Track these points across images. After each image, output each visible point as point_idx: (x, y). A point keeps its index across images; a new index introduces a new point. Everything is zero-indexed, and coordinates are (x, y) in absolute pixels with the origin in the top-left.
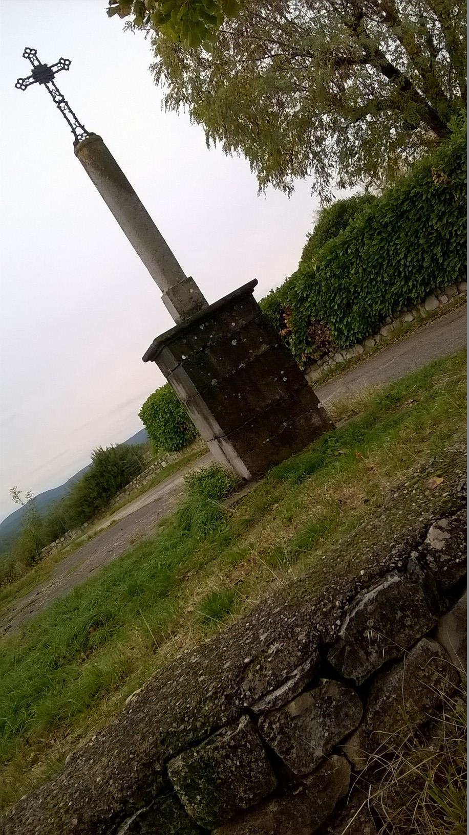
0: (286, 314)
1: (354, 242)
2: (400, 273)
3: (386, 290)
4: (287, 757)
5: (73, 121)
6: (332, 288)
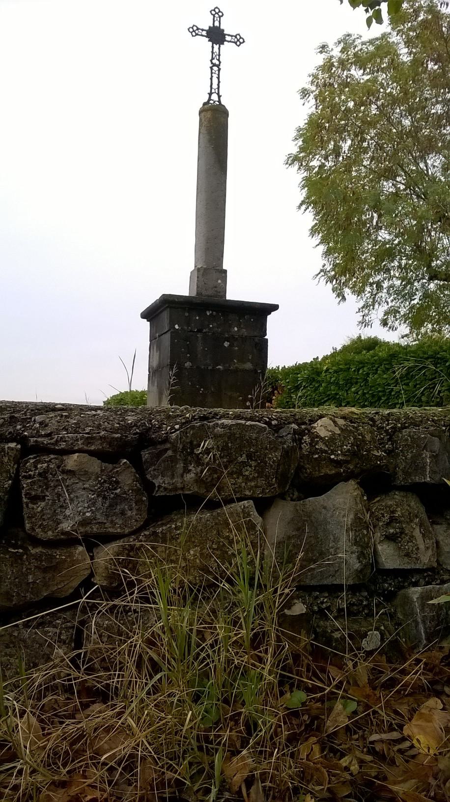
0: (278, 391)
4: (30, 505)
5: (215, 86)
6: (328, 393)
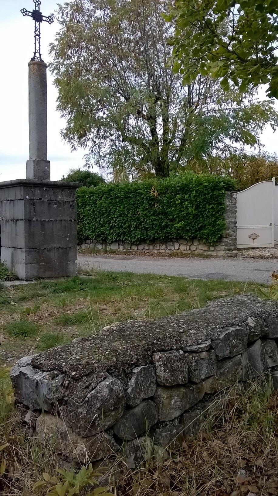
1: (97, 195)
2: (110, 223)
3: (98, 227)
5: (37, 48)
